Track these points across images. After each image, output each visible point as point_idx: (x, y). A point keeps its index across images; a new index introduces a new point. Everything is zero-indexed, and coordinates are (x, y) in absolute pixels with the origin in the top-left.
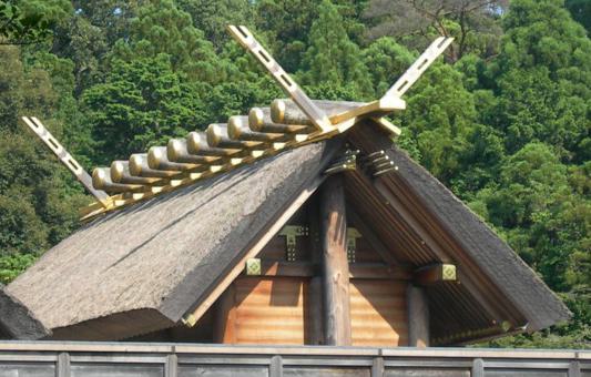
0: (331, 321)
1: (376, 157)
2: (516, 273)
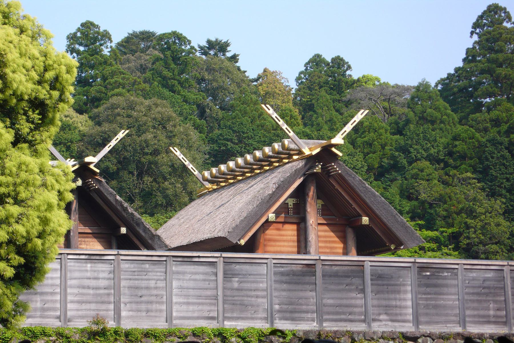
0: (309, 243)
1: (329, 167)
2: (397, 221)
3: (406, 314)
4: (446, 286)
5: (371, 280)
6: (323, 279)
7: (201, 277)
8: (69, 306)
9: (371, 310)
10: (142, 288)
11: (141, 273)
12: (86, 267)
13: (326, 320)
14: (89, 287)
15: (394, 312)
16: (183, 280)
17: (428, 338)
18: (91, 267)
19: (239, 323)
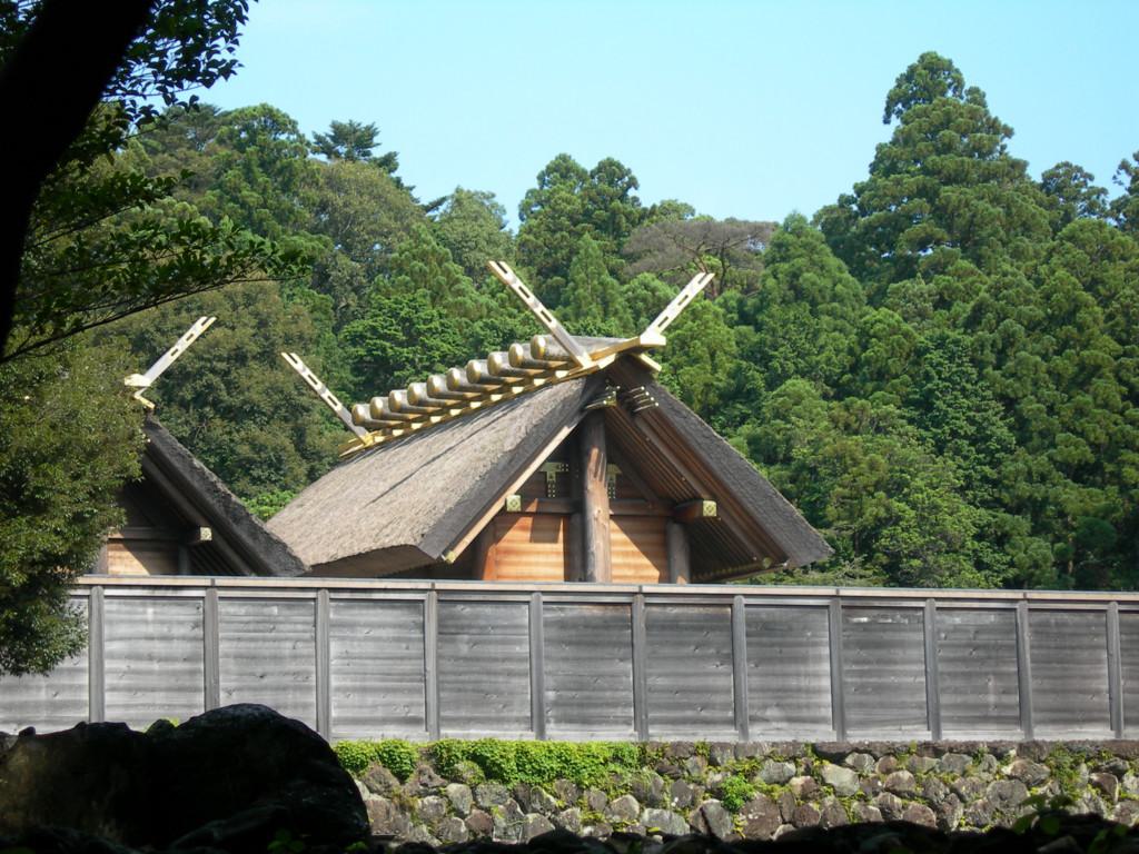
0: (591, 557)
1: (637, 393)
3: (819, 706)
4: (902, 644)
5: (747, 635)
6: (647, 635)
7: (391, 633)
8: (109, 698)
9: (749, 699)
10: (265, 658)
11: (261, 627)
12: (145, 613)
13: (656, 721)
14: (151, 658)
15: (794, 701)
16: (353, 639)
17: (866, 755)
18: (155, 613)
19: (472, 731)
